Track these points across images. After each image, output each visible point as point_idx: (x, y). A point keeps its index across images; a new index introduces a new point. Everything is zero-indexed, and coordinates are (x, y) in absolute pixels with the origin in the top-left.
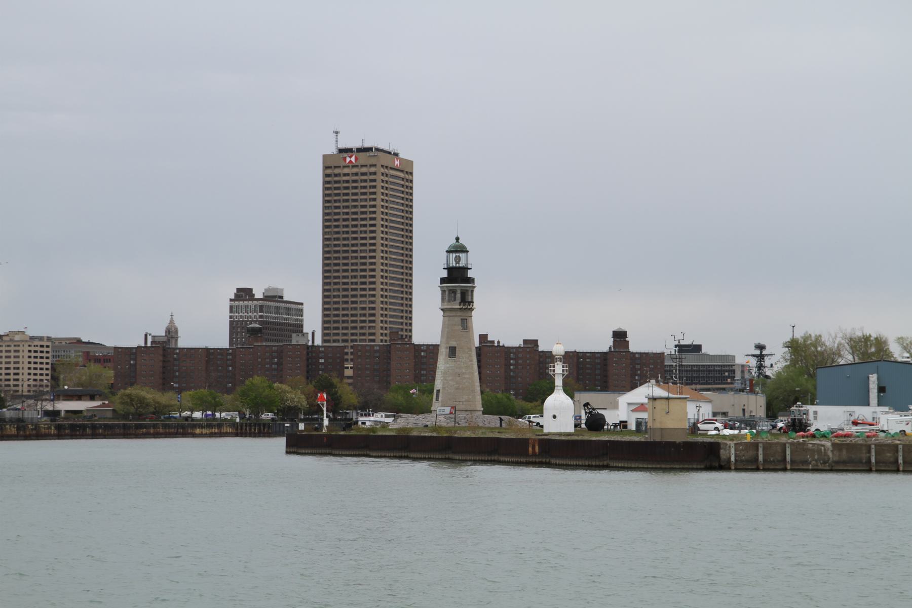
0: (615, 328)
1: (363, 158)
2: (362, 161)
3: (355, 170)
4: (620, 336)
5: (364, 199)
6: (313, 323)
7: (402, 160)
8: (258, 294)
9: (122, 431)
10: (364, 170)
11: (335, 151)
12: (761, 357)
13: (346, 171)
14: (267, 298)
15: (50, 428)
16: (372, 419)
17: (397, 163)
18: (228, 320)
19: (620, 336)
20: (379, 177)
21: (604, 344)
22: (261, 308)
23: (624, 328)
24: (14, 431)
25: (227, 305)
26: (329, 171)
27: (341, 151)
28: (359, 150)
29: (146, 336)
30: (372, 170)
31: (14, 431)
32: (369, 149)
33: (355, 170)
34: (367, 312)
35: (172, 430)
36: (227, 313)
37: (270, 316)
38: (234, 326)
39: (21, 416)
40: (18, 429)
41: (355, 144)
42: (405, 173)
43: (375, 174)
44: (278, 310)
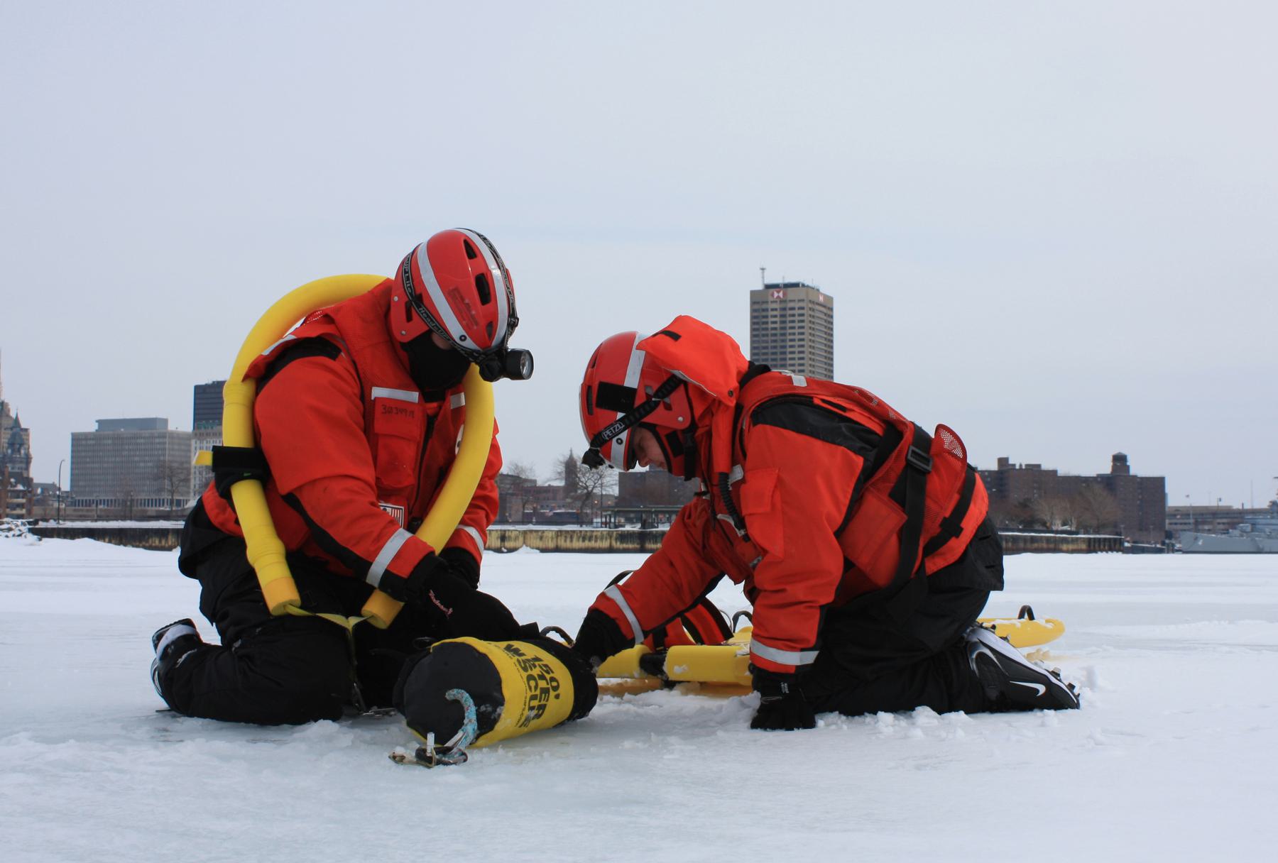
0: (1115, 452)
4: (1120, 460)
17: (821, 298)
19: (1120, 460)
23: (1124, 452)
26: (756, 307)
27: (768, 287)
28: (787, 286)
30: (801, 304)
32: (796, 285)
42: (827, 308)
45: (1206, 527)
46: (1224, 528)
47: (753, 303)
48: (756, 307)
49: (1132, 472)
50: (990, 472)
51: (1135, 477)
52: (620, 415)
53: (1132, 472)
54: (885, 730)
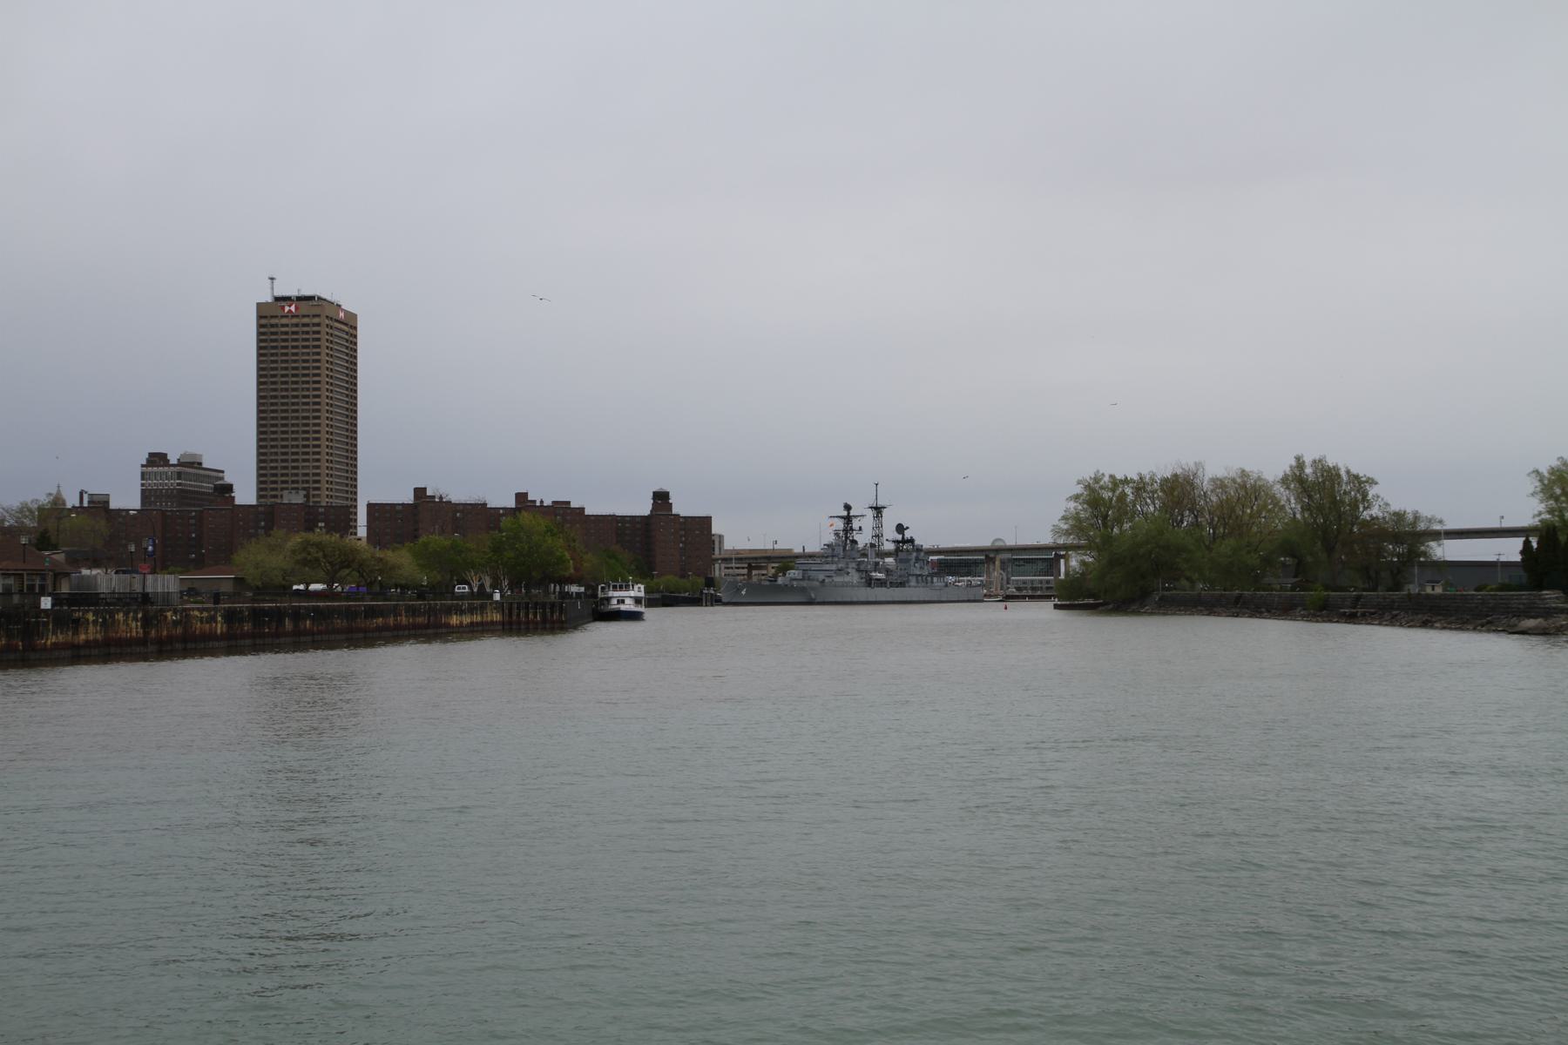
0: (656, 489)
1: (305, 308)
2: (303, 311)
3: (295, 321)
4: (661, 498)
5: (304, 353)
6: (246, 494)
7: (346, 312)
8: (173, 460)
9: (345, 623)
10: (306, 320)
11: (270, 300)
12: (848, 519)
13: (284, 321)
14: (180, 464)
15: (213, 619)
16: (632, 593)
17: (342, 315)
18: (139, 488)
19: (661, 498)
20: (324, 329)
21: (644, 508)
22: (179, 475)
23: (666, 488)
24: (135, 629)
25: (139, 470)
26: (263, 321)
27: (277, 299)
28: (300, 299)
29: (81, 494)
30: (316, 320)
31: (135, 629)
32: (311, 298)
33: (295, 321)
34: (312, 478)
35: (420, 620)
36: (139, 481)
37: (190, 484)
38: (146, 495)
39: (138, 588)
40: (147, 622)
41: (293, 293)
42: (349, 325)
43: (318, 325)
44: (198, 478)
45: (454, 620)
46: (774, 579)
47: (260, 317)
48: (263, 321)
49: (675, 511)
50: (633, 519)
51: (677, 516)
52: (1535, 545)
53: (675, 511)
54: (1074, 563)
